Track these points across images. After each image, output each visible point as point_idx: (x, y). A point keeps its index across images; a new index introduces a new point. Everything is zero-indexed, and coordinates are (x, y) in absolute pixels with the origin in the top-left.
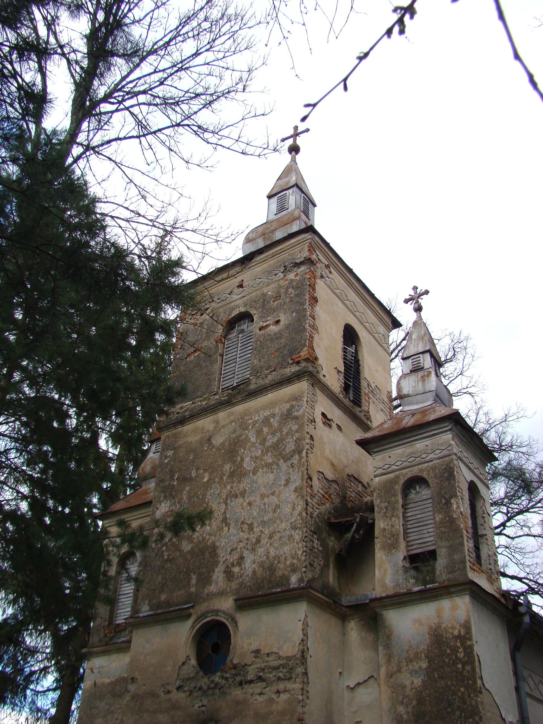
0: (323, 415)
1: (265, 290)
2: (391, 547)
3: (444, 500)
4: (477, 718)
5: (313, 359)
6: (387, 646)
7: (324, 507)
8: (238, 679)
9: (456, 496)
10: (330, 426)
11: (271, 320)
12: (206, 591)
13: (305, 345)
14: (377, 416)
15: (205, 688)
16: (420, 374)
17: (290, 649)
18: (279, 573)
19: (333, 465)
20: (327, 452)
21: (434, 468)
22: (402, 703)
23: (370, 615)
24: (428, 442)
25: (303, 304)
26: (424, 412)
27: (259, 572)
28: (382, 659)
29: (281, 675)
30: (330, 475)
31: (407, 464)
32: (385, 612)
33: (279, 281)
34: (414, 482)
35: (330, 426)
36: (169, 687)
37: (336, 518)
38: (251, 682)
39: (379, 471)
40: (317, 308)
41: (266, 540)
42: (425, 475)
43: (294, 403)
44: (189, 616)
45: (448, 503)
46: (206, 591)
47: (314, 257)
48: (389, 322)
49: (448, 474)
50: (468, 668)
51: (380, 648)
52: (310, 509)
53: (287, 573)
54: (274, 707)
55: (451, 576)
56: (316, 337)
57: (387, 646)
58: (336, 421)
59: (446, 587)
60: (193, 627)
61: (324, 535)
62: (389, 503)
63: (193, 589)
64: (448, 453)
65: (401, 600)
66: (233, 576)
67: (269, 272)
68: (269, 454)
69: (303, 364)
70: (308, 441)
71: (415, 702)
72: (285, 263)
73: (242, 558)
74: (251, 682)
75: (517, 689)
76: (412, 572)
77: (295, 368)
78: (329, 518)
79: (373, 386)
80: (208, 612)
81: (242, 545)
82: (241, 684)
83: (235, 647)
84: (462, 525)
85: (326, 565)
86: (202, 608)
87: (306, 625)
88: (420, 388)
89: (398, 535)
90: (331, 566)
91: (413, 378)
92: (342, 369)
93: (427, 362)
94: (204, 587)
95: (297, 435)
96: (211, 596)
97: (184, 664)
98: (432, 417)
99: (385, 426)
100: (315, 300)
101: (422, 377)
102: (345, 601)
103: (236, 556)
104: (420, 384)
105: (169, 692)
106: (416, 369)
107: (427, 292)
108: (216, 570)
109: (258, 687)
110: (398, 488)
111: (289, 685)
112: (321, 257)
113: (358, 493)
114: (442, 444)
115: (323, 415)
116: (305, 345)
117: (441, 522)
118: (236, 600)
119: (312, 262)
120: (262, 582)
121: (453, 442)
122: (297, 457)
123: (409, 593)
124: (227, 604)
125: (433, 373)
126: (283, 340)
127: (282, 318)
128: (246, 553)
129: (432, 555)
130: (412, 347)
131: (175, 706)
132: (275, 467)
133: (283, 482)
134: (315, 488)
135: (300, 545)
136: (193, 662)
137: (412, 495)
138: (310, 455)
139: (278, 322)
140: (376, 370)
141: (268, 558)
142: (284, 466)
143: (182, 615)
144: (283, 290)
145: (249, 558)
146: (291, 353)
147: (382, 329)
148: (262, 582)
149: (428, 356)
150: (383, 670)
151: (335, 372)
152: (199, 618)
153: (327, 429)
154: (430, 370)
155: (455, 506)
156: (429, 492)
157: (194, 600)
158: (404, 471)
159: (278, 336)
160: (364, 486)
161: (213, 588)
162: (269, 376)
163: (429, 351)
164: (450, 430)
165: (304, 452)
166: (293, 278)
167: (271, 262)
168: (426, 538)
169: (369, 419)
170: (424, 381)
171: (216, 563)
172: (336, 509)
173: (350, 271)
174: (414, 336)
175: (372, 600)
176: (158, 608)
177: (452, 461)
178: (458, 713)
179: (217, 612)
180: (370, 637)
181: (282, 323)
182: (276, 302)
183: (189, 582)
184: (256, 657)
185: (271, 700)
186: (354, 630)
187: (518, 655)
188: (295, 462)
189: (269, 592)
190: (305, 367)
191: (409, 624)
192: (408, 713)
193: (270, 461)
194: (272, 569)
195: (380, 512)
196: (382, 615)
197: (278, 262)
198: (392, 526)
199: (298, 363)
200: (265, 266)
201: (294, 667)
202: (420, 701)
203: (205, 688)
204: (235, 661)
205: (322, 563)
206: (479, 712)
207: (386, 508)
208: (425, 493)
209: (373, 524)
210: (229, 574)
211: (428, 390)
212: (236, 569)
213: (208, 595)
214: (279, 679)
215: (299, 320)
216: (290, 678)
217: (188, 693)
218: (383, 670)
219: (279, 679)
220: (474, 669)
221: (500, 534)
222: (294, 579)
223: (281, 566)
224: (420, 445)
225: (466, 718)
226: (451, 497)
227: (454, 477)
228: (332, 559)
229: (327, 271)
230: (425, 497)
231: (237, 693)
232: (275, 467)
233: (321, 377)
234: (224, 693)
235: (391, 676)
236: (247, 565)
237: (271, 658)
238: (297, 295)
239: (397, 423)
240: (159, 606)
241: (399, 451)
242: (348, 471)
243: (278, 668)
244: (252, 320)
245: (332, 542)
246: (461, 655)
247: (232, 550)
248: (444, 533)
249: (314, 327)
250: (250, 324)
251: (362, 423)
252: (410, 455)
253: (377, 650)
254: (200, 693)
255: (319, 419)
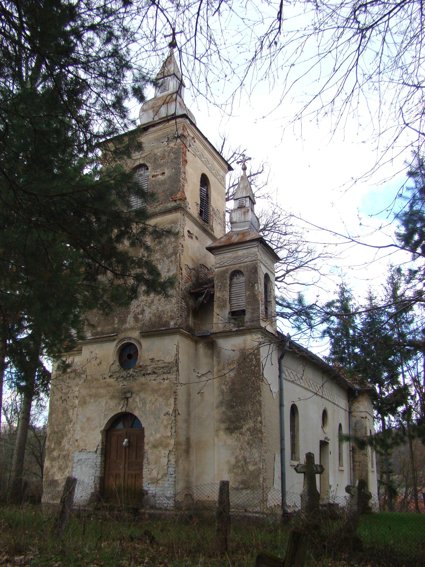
0: (189, 231)
1: (156, 151)
2: (222, 307)
3: (251, 284)
4: (259, 391)
5: (184, 199)
6: (218, 357)
7: (188, 284)
8: (143, 372)
9: (258, 283)
10: (192, 237)
11: (159, 172)
12: (124, 327)
13: (179, 191)
14: (217, 227)
15: (125, 376)
16: (243, 210)
17: (170, 359)
18: (164, 320)
19: (193, 260)
20: (190, 253)
21: (247, 266)
22: (224, 384)
23: (209, 341)
24: (245, 251)
25: (179, 164)
26: (244, 234)
27: (153, 318)
28: (215, 363)
29: (165, 371)
30: (191, 266)
31: (232, 263)
32: (217, 340)
33: (164, 147)
34: (236, 273)
35: (192, 237)
36: (105, 376)
37: (193, 289)
38: (150, 374)
39: (218, 265)
40: (187, 167)
41: (157, 302)
42: (242, 270)
43: (173, 225)
44: (115, 340)
45: (253, 286)
46: (124, 327)
47: (186, 134)
48: (226, 167)
49: (254, 270)
50: (257, 368)
51: (215, 358)
52: (181, 286)
53: (168, 320)
54: (162, 386)
55: (252, 324)
56: (186, 185)
57: (218, 357)
58: (195, 234)
59: (249, 329)
60: (117, 346)
61: (188, 299)
62: (222, 283)
63: (116, 326)
64: (255, 259)
65: (227, 334)
66: (139, 320)
67: (158, 140)
68: (158, 254)
69: (178, 202)
70: (181, 248)
71: (230, 384)
72: (168, 135)
73: (143, 310)
74: (150, 374)
75: (280, 377)
76: (233, 321)
77: (173, 204)
78: (190, 290)
79: (215, 210)
80: (125, 338)
81: (143, 303)
82: (144, 375)
83: (140, 357)
84: (259, 298)
85: (188, 316)
86: (122, 336)
87: (178, 347)
88: (242, 219)
89: (226, 301)
90: (191, 315)
91: (239, 212)
92: (199, 202)
93: (248, 204)
94: (122, 325)
95: (174, 244)
96: (126, 330)
97: (112, 364)
98: (248, 238)
99: (222, 240)
100: (186, 161)
101: (244, 212)
102: (197, 334)
103: (140, 309)
104: (243, 216)
105: (105, 378)
106: (241, 207)
107: (250, 159)
108: (129, 316)
109: (153, 377)
110: (228, 275)
111: (169, 376)
112: (190, 133)
113: (205, 274)
114: (252, 254)
115: (189, 231)
116: (179, 191)
117: (249, 296)
118: (141, 333)
119: (185, 137)
120: (155, 324)
121: (258, 253)
122: (174, 257)
123: (230, 331)
124: (136, 334)
125: (250, 210)
126: (167, 186)
127: (166, 171)
128: (145, 308)
129: (243, 312)
130: (239, 193)
131: (109, 385)
132: (161, 261)
133: (166, 270)
134: (184, 274)
135: (176, 306)
136: (118, 363)
137: (235, 280)
138: (182, 256)
139: (163, 173)
140: (218, 200)
141: (158, 311)
142: (167, 261)
143: (110, 339)
144: (166, 153)
145: (147, 311)
146: (171, 195)
147: (222, 173)
148: (155, 324)
149: (248, 199)
150: (215, 369)
151: (195, 205)
152: (120, 341)
153: (190, 239)
154: (249, 208)
155: (256, 288)
156: (244, 279)
157: (117, 331)
158: (231, 266)
159: (163, 183)
160: (208, 269)
161: (127, 326)
162: (158, 207)
163: (249, 197)
164: (258, 246)
165: (178, 254)
166: (173, 146)
167: (160, 133)
168: (241, 303)
169: (212, 230)
170: (245, 215)
171: (129, 313)
172: (193, 284)
173: (206, 139)
174: (241, 186)
175: (211, 334)
176: (96, 335)
177: (257, 263)
178: (250, 389)
179: (130, 338)
180: (210, 352)
181: (166, 174)
182: (163, 161)
183: (114, 322)
184: (152, 362)
185: (160, 383)
186: (202, 349)
187: (283, 361)
188: (173, 260)
189: (158, 329)
190: (179, 204)
191: (230, 346)
192: (227, 389)
193: (159, 257)
194: (160, 317)
195: (217, 288)
196: (215, 341)
197: (164, 134)
198: (224, 296)
199: (175, 201)
200: (156, 135)
201: (172, 367)
202: (233, 383)
203: (125, 376)
204: (141, 364)
205: (186, 314)
206: (260, 389)
207: (221, 286)
208: (242, 279)
209: (214, 294)
210: (136, 319)
211: (247, 220)
212: (140, 316)
213: (125, 329)
214: (164, 373)
215: (176, 174)
216: (170, 373)
217: (115, 379)
218: (215, 369)
219: (164, 373)
220: (260, 369)
221: (281, 281)
222: (172, 323)
223: (165, 316)
224: (240, 253)
225: (254, 391)
226: (255, 283)
227: (257, 273)
228: (191, 312)
229: (193, 141)
230: (242, 281)
231: (142, 379)
232: (161, 261)
233: (188, 209)
234: (135, 379)
235: (220, 371)
236: (146, 315)
237: (159, 363)
238: (175, 158)
239: (229, 239)
240: (97, 334)
241: (229, 255)
242: (200, 262)
243: (164, 368)
244: (147, 169)
245: (191, 303)
246: (254, 363)
247: (138, 306)
248: (250, 301)
249: (185, 179)
250: (146, 171)
251: (208, 233)
252: (235, 258)
253: (213, 359)
254: (122, 379)
255: (186, 234)
